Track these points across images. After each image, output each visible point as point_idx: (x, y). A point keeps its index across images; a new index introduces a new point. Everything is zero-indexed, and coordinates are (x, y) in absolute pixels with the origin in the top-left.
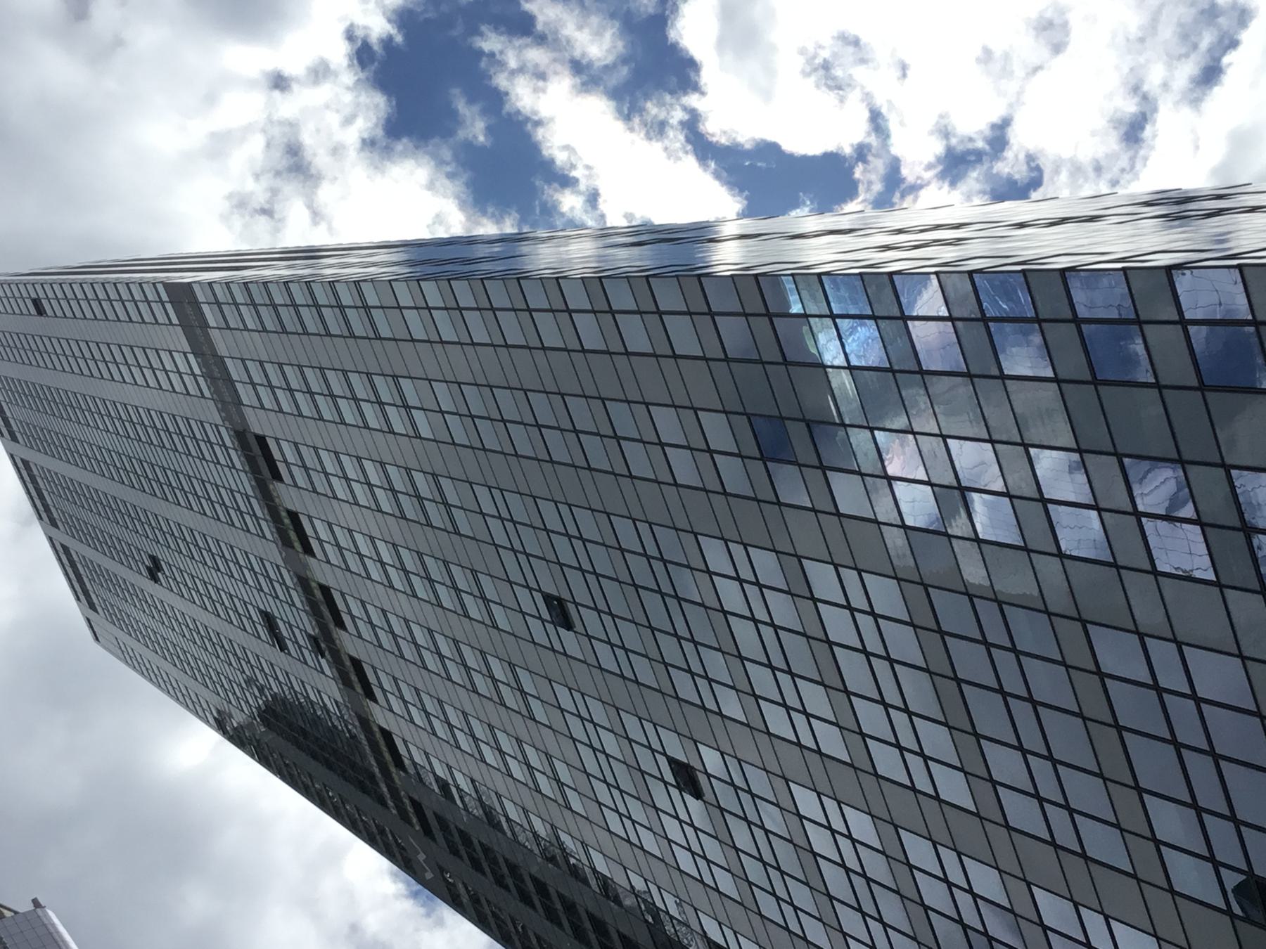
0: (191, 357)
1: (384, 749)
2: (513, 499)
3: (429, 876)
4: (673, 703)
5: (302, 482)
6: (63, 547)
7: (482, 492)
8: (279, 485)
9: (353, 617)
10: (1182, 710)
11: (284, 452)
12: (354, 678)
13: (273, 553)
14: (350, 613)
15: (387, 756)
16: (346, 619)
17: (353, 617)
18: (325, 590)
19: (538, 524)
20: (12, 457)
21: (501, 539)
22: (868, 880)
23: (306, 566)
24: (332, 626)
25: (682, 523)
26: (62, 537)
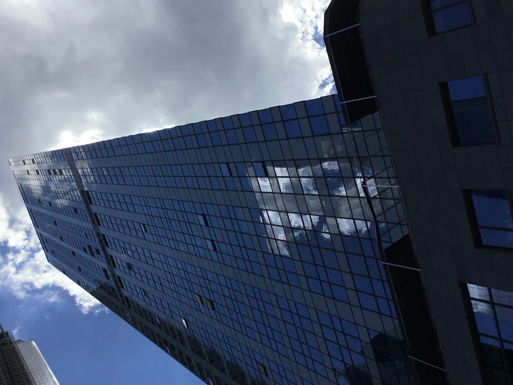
0: (70, 170)
1: (118, 282)
2: (170, 259)
3: (130, 320)
4: (210, 318)
5: (106, 226)
6: (40, 234)
7: (162, 256)
8: (108, 248)
9: (126, 286)
10: (336, 320)
11: (101, 218)
12: (111, 261)
13: (90, 226)
14: (110, 242)
15: (119, 284)
16: (124, 286)
17: (126, 286)
18: (119, 278)
19: (166, 237)
20: (37, 232)
21: (166, 269)
22: (245, 326)
23: (98, 229)
24: (105, 247)
25: (213, 271)
26: (40, 231)
